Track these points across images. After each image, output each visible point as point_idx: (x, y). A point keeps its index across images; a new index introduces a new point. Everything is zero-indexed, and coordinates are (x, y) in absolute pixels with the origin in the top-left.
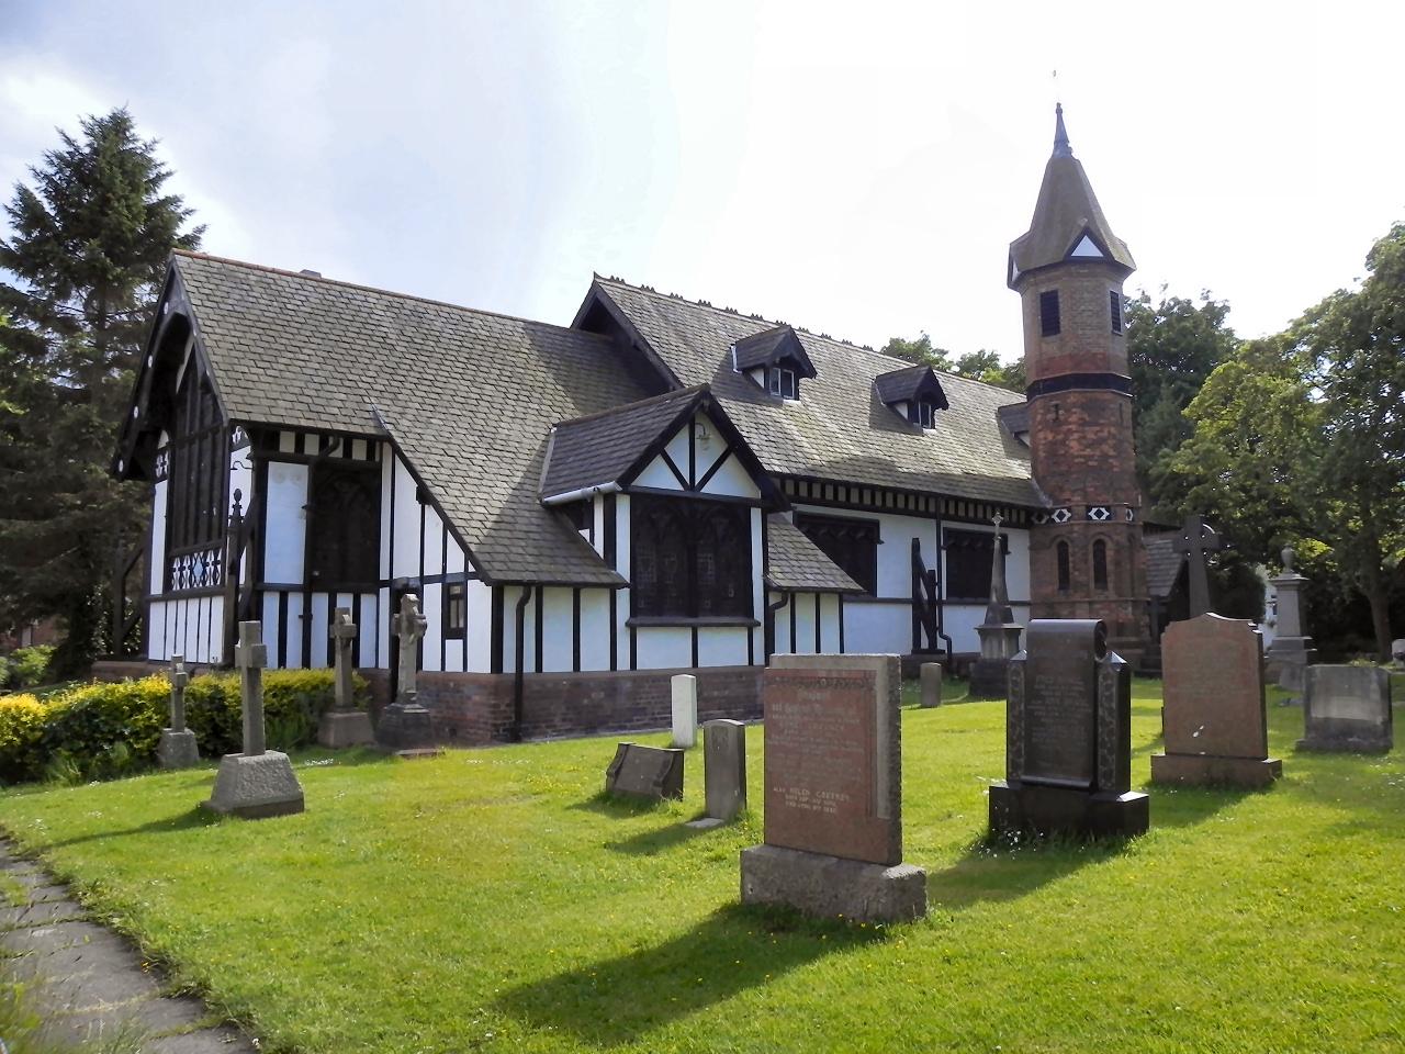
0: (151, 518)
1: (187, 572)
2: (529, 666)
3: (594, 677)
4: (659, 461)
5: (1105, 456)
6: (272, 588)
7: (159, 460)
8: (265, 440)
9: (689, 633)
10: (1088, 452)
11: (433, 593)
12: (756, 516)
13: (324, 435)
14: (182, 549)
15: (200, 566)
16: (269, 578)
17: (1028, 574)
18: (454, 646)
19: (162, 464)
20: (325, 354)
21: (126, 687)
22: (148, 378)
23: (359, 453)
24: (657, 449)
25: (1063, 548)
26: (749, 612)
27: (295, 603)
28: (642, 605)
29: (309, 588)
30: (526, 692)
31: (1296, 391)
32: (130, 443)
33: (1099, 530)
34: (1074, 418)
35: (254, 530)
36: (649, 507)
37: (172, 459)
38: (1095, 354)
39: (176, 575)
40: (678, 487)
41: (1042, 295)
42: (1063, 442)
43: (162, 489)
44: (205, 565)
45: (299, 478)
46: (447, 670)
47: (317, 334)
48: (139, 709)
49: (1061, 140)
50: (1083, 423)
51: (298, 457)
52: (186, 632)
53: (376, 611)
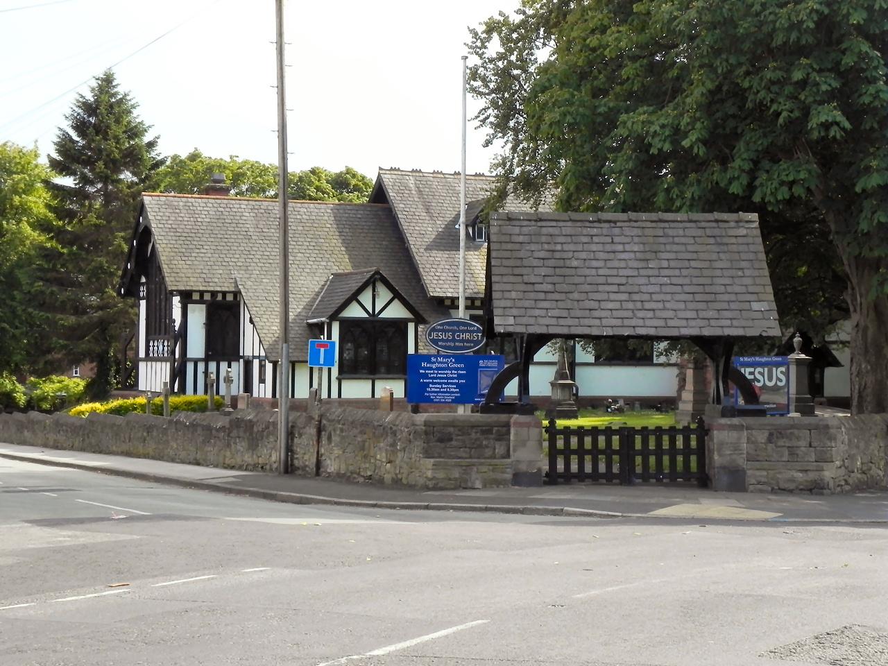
0: (138, 315)
1: (156, 348)
2: (334, 395)
4: (354, 304)
6: (191, 360)
8: (187, 297)
9: (370, 382)
11: (256, 362)
12: (411, 327)
13: (214, 294)
14: (153, 336)
15: (160, 347)
16: (189, 355)
18: (262, 385)
19: (143, 291)
20: (215, 248)
21: (130, 401)
22: (134, 250)
24: (354, 297)
27: (201, 366)
28: (345, 369)
29: (207, 360)
32: (126, 280)
35: (183, 335)
37: (147, 289)
39: (151, 348)
40: (366, 315)
43: (143, 303)
45: (202, 311)
46: (296, 397)
47: (212, 236)
48: (135, 409)
51: (201, 301)
52: (153, 377)
53: (237, 369)
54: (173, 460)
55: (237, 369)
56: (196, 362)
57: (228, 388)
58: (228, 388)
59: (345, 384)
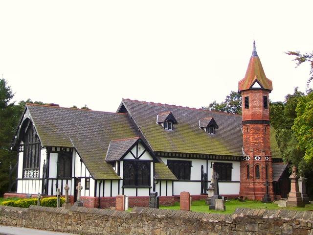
1: (29, 174)
2: (101, 195)
3: (107, 198)
4: (130, 154)
5: (260, 143)
6: (51, 179)
7: (20, 147)
9: (135, 190)
10: (255, 141)
11: (83, 180)
12: (152, 164)
13: (61, 148)
16: (50, 177)
17: (240, 175)
22: (19, 131)
23: (68, 150)
24: (129, 151)
25: (248, 166)
26: (150, 185)
27: (55, 182)
29: (57, 179)
30: (101, 200)
31: (67, 198)
33: (257, 162)
34: (251, 132)
35: (47, 169)
36: (127, 163)
38: (258, 115)
40: (134, 158)
41: (245, 97)
42: (249, 138)
44: (34, 173)
49: (255, 53)
50: (254, 133)
53: (71, 183)
54: (6, 225)
55: (71, 183)
56: (53, 179)
57: (67, 191)
58: (67, 191)
59: (125, 190)
